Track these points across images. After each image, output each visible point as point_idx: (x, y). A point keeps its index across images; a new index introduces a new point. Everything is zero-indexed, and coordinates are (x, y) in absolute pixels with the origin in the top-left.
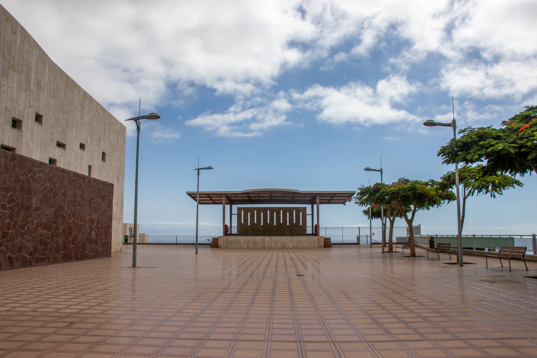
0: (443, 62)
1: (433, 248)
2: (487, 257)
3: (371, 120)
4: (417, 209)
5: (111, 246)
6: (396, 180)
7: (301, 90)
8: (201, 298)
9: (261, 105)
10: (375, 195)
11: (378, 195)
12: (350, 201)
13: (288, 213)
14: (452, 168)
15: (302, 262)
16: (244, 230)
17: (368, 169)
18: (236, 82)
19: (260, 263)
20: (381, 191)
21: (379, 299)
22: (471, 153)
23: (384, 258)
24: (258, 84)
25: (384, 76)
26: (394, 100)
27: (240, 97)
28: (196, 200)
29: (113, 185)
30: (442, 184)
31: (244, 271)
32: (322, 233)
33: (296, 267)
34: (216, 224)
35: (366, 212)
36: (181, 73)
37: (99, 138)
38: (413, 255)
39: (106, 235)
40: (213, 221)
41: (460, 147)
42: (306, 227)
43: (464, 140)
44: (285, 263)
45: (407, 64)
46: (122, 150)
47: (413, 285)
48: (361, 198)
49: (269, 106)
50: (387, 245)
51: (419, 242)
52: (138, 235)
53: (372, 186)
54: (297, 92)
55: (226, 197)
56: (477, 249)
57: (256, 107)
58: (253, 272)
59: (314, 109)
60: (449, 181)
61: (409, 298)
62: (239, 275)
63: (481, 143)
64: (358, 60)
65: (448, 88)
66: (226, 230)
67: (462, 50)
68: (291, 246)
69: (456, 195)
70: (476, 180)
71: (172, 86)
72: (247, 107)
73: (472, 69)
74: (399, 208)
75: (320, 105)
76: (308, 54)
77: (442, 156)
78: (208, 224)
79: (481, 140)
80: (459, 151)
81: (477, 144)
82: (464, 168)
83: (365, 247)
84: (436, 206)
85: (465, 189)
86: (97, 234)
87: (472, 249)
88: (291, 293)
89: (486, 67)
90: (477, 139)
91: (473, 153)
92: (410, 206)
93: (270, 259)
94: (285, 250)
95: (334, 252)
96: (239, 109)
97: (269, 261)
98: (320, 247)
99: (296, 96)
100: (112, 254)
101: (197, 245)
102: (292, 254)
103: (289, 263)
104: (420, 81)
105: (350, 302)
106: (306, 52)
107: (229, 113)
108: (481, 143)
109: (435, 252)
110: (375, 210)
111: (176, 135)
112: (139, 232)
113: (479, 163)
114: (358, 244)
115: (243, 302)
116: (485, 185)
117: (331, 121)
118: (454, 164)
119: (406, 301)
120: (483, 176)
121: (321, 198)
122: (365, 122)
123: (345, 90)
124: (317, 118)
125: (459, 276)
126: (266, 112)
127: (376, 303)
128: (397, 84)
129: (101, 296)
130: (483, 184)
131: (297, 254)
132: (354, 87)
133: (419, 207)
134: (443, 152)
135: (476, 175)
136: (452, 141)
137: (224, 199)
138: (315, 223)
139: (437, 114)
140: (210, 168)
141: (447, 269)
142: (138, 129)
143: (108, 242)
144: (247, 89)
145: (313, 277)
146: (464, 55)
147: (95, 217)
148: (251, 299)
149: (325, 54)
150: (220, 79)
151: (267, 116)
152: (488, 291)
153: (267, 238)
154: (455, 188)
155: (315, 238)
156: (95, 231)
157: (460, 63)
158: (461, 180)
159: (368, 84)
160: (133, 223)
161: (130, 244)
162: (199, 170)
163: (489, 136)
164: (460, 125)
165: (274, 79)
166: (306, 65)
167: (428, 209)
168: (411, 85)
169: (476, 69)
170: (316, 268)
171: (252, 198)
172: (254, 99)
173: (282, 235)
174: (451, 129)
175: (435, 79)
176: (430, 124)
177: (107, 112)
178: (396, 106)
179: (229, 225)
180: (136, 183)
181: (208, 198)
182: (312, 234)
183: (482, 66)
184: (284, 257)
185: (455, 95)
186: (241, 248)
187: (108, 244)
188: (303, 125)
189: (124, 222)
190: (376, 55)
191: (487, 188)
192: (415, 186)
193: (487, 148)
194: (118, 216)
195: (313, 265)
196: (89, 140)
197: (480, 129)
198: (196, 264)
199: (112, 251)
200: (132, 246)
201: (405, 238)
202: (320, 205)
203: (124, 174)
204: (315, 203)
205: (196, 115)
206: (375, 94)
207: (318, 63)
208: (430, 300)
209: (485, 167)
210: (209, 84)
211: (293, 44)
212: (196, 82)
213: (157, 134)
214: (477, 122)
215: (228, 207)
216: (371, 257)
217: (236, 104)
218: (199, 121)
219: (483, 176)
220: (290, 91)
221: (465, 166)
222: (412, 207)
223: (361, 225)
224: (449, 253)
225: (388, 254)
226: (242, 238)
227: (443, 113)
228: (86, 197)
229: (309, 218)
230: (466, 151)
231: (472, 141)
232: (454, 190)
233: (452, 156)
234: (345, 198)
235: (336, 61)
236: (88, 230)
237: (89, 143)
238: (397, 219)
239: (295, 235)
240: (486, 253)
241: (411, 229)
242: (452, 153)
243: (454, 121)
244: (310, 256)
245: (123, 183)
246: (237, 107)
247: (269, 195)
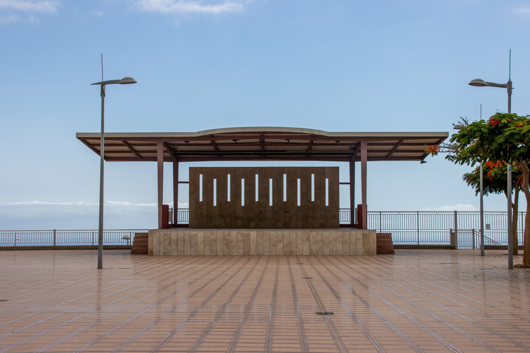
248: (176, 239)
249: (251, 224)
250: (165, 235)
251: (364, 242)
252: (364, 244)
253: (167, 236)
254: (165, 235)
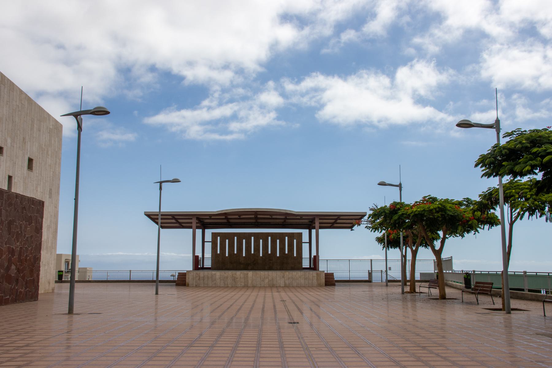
0: (484, 41)
1: (470, 288)
2: (544, 301)
3: (386, 119)
4: (447, 236)
5: (38, 286)
6: (419, 199)
7: (296, 80)
8: (161, 355)
9: (245, 98)
10: (392, 218)
11: (396, 217)
12: (359, 225)
13: (278, 241)
14: (494, 182)
15: (296, 305)
16: (221, 263)
17: (382, 184)
18: (212, 67)
19: (241, 307)
20: (400, 213)
21: (398, 355)
22: (520, 163)
23: (404, 300)
24: (240, 71)
25: (406, 61)
26: (417, 93)
27: (217, 88)
28: (157, 223)
29: (43, 203)
30: (480, 203)
31: (220, 317)
32: (322, 267)
33: (288, 311)
34: (183, 255)
35: (380, 240)
36: (137, 54)
37: (24, 139)
38: (443, 297)
39: (32, 271)
40: (179, 251)
41: (506, 154)
42: (301, 258)
43: (512, 146)
44: (274, 306)
45: (436, 45)
46: (57, 154)
47: (443, 337)
48: (374, 221)
49: (255, 100)
50: (408, 284)
51: (450, 280)
52: (77, 269)
53: (388, 205)
54: (291, 82)
55: (198, 218)
56: (529, 291)
57: (238, 101)
58: (232, 319)
59: (313, 104)
60: (490, 199)
61: (438, 355)
62: (213, 323)
63: (535, 150)
64: (372, 40)
65: (491, 77)
66: (197, 263)
67: (512, 25)
68: (282, 284)
69: (499, 218)
70: (527, 200)
71: (125, 71)
72: (225, 101)
73: (525, 51)
74: (423, 234)
75: (321, 99)
76: (307, 31)
77: (481, 167)
78: (173, 254)
79: (534, 146)
80: (504, 161)
81: (529, 151)
82: (511, 183)
83: (379, 285)
84: (473, 232)
85: (511, 210)
86: (18, 270)
87: (523, 290)
88: (282, 346)
89: (544, 48)
90: (529, 145)
91: (522, 163)
92: (438, 232)
93: (255, 301)
94: (274, 290)
95: (339, 291)
96: (214, 104)
97: (254, 304)
98: (320, 285)
99: (290, 87)
100: (39, 297)
101: (157, 282)
102: (283, 294)
103: (280, 306)
104: (453, 67)
105: (360, 359)
106: (302, 29)
107: (201, 108)
108: (535, 150)
109: (472, 293)
110: (392, 237)
111: (131, 137)
112: (79, 265)
113: (532, 176)
114: (370, 281)
115: (218, 359)
116: (539, 206)
117: (335, 120)
118: (497, 178)
119: (434, 359)
120: (537, 194)
121: (321, 221)
122: (379, 121)
123: (353, 80)
124: (316, 116)
125: (506, 327)
126: (251, 108)
127: (394, 361)
128: (422, 72)
129: (21, 357)
130: (536, 205)
131: (290, 294)
132: (366, 76)
133: (450, 234)
134: (482, 162)
135: (526, 193)
136: (494, 147)
137: (194, 221)
138: (314, 253)
139: (474, 112)
140: (176, 181)
141: (489, 316)
142: (79, 127)
143: (34, 280)
144: (226, 77)
145: (311, 325)
146: (514, 32)
147: (16, 246)
148: (228, 355)
149: (328, 32)
150: (191, 64)
151: (251, 112)
152: (548, 349)
153: (250, 273)
154: (498, 208)
155: (314, 273)
156: (16, 266)
157: (508, 44)
158: (506, 200)
159: (383, 72)
160: (71, 253)
161: (65, 282)
162: (161, 183)
163: (545, 141)
164: (507, 126)
165: (261, 65)
166: (303, 46)
167: (463, 236)
168: (441, 73)
169: (530, 51)
170: (315, 313)
171: (231, 221)
172: (234, 90)
173: (270, 269)
174: (494, 131)
175: (474, 65)
176: (465, 125)
177: (35, 103)
178: (420, 101)
179: (200, 256)
180: (76, 199)
181: (174, 221)
182: (310, 269)
183: (539, 47)
184: (273, 298)
185: (499, 87)
186: (216, 287)
187: (34, 283)
188: (298, 125)
189: (58, 252)
190: (396, 33)
191: (543, 209)
192: (444, 206)
193: (543, 157)
194: (50, 245)
195: (311, 310)
196: (9, 141)
197: (534, 131)
198: (156, 309)
199: (40, 292)
200: (69, 284)
201: (432, 274)
202: (321, 231)
203: (59, 188)
204: (314, 228)
205: (157, 111)
206: (393, 85)
207: (319, 44)
208: (467, 359)
209: (539, 181)
210: (175, 70)
211: (286, 18)
212: (158, 66)
213: (105, 135)
214: (529, 122)
215: (199, 232)
216: (387, 299)
217: (211, 97)
218: (161, 118)
219: (537, 194)
220: (282, 80)
221: (511, 181)
222: (441, 233)
223: (373, 257)
224: (492, 295)
225: (409, 295)
226: (218, 274)
227: (484, 110)
228: (3, 220)
229: (305, 247)
230: (513, 160)
231: (522, 147)
232: (497, 212)
233: (494, 167)
234: (354, 221)
235: (343, 41)
236: (6, 265)
237: (9, 145)
238: (421, 249)
239: (286, 269)
240: (542, 296)
241: (439, 263)
242: (496, 162)
243: (498, 121)
244: (306, 297)
245: (57, 200)
246: (212, 101)
247: (253, 216)
252: (317, 280)
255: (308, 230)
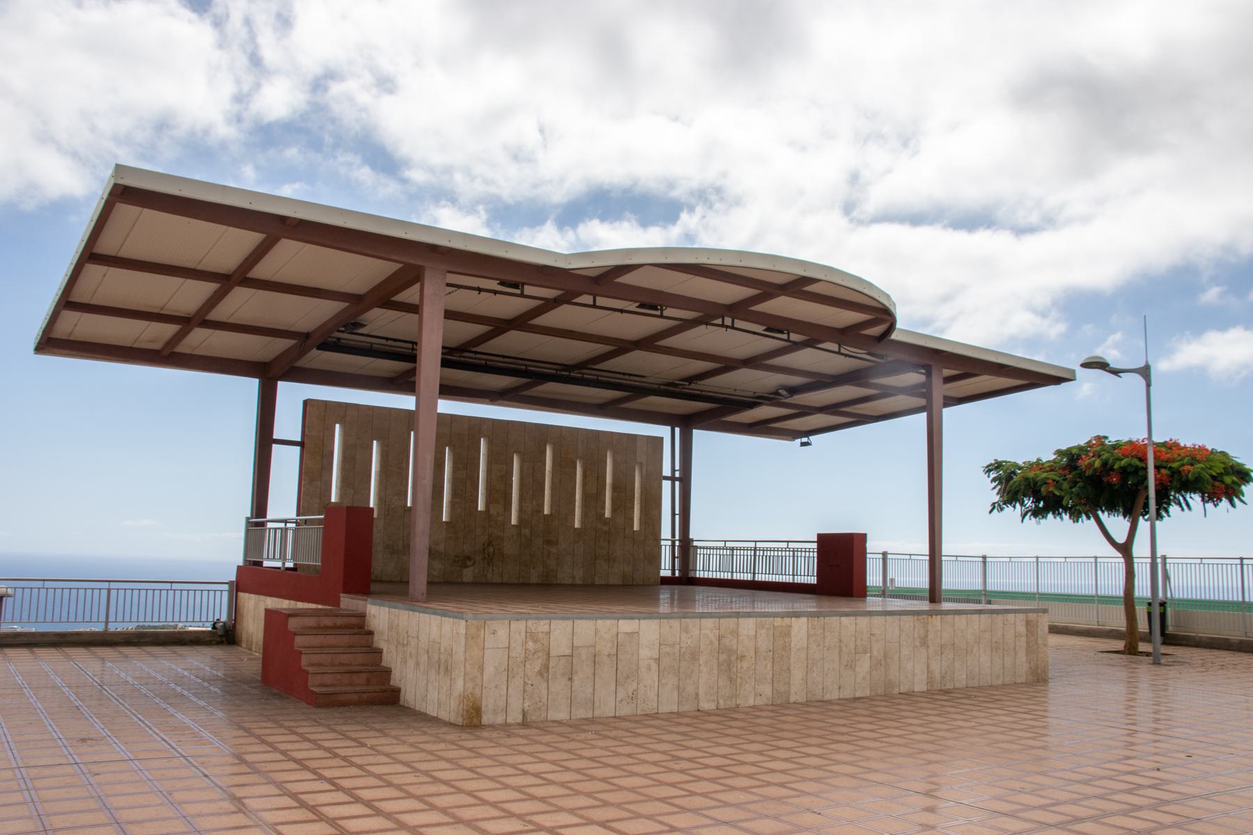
248: (568, 652)
249: (465, 571)
250: (530, 635)
251: (1028, 643)
252: (1029, 651)
253: (535, 641)
254: (530, 635)
255: (299, 439)
